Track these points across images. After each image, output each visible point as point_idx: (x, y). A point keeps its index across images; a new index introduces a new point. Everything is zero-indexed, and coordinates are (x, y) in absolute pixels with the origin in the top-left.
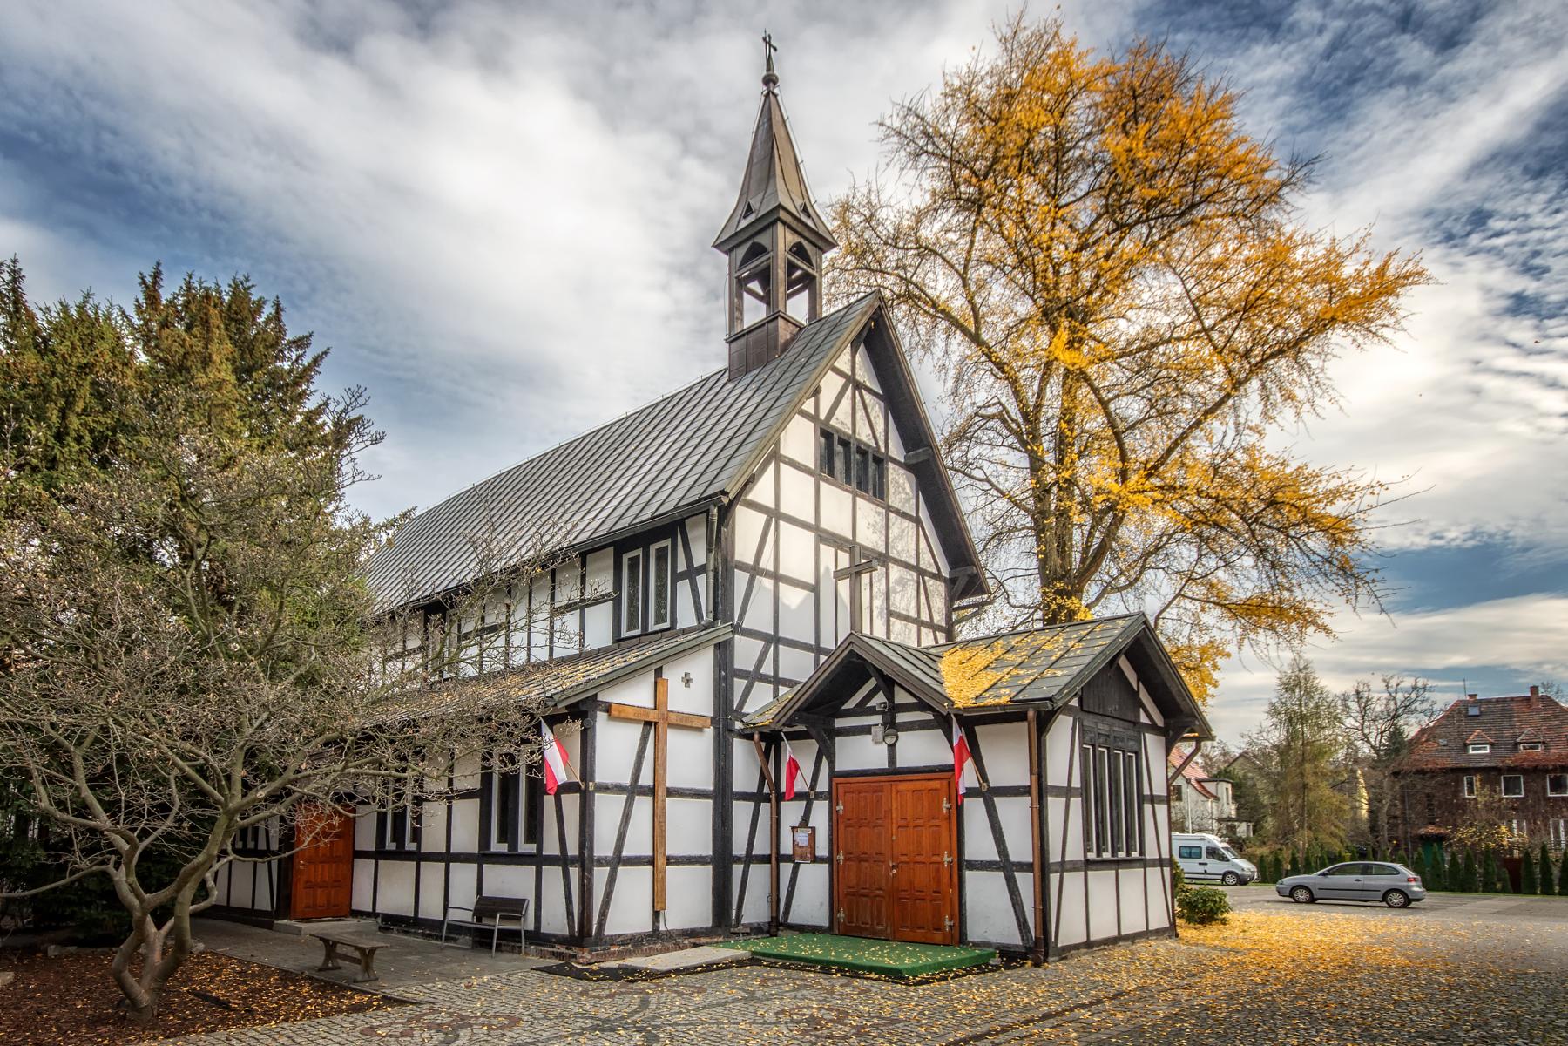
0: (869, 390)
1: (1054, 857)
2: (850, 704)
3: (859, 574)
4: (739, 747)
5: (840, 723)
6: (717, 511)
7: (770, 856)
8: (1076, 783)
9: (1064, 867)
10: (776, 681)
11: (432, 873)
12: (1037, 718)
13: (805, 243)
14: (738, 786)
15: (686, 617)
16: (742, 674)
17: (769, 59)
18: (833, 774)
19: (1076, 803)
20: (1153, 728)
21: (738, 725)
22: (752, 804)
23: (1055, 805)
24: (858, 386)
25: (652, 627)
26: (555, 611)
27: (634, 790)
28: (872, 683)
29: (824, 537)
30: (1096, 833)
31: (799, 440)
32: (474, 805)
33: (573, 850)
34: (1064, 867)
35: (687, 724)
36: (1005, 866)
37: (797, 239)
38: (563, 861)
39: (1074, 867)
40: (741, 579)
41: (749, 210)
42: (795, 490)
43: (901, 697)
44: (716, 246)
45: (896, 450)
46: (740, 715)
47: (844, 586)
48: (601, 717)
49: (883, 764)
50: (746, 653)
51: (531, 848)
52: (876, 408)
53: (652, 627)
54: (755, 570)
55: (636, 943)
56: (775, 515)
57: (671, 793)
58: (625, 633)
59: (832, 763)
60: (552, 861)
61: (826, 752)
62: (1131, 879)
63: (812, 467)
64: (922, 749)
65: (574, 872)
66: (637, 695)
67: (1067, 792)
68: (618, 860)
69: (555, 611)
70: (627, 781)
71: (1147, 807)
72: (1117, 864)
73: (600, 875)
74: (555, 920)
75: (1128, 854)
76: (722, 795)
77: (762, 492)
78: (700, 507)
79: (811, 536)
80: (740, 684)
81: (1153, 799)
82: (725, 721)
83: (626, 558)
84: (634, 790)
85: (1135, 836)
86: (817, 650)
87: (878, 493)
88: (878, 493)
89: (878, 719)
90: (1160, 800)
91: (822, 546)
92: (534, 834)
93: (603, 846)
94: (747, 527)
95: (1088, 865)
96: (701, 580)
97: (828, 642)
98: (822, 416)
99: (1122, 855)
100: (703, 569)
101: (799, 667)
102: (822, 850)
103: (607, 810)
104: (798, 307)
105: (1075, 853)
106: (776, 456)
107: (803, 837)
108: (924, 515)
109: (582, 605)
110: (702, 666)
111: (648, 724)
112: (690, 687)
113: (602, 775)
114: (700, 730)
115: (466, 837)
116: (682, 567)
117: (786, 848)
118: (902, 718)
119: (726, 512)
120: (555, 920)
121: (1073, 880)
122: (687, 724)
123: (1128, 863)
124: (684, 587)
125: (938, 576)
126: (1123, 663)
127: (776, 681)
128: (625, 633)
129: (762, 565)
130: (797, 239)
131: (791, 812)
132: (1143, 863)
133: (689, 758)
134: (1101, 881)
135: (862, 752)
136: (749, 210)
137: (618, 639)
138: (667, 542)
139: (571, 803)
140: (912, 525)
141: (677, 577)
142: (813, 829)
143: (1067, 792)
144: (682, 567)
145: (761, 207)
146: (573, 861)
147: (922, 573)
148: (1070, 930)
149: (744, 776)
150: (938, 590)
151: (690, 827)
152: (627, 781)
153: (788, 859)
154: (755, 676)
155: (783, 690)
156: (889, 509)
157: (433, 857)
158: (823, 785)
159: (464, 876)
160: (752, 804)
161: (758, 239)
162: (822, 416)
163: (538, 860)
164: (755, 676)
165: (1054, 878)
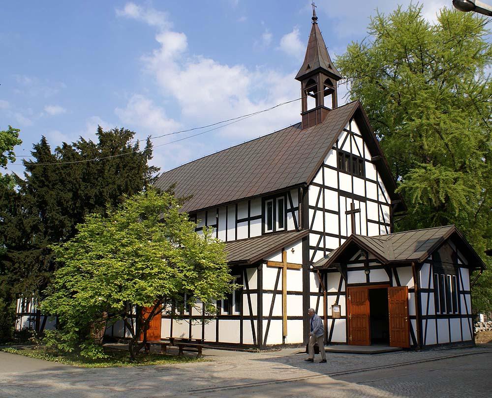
0: (357, 135)
1: (424, 313)
2: (353, 259)
3: (354, 213)
4: (312, 275)
5: (349, 266)
6: (302, 190)
8: (432, 287)
9: (428, 317)
10: (324, 249)
12: (415, 266)
13: (330, 79)
14: (311, 291)
15: (291, 226)
16: (312, 248)
17: (314, 11)
18: (347, 285)
19: (432, 295)
20: (464, 266)
21: (311, 267)
22: (317, 297)
23: (424, 296)
24: (353, 134)
25: (278, 229)
26: (237, 221)
27: (275, 292)
28: (359, 252)
29: (341, 193)
31: (332, 159)
33: (255, 313)
34: (428, 317)
35: (293, 267)
37: (327, 78)
38: (251, 318)
39: (432, 317)
40: (311, 212)
41: (309, 67)
42: (330, 177)
43: (371, 257)
44: (297, 78)
45: (368, 156)
46: (312, 263)
47: (349, 216)
48: (264, 266)
49: (300, 323)
50: (313, 240)
51: (237, 313)
52: (360, 141)
53: (278, 229)
54: (316, 208)
55: (276, 347)
56: (323, 187)
57: (289, 293)
58: (267, 231)
59: (346, 281)
60: (464, 316)
61: (345, 277)
62: (455, 322)
63: (336, 167)
64: (378, 276)
65: (255, 322)
66: (278, 258)
67: (428, 291)
68: (271, 318)
69: (237, 221)
70: (273, 289)
71: (462, 296)
72: (449, 317)
73: (265, 322)
74: (248, 340)
76: (306, 294)
77: (318, 180)
78: (297, 186)
79: (336, 193)
80: (311, 252)
81: (464, 293)
82: (307, 265)
83: (266, 202)
84: (275, 292)
85: (457, 306)
86: (340, 237)
87: (361, 174)
88: (361, 174)
89: (362, 265)
90: (467, 292)
91: (341, 197)
92: (240, 308)
93: (266, 313)
94: (313, 191)
96: (296, 213)
97: (343, 234)
98: (339, 147)
99: (451, 313)
100: (297, 209)
101: (333, 244)
102: (343, 314)
103: (267, 298)
104: (328, 102)
105: (432, 312)
106: (323, 165)
107: (337, 310)
108: (380, 180)
109: (249, 219)
110: (299, 247)
111: (280, 268)
112: (295, 255)
113: (265, 287)
114: (298, 270)
116: (289, 207)
117: (330, 314)
118: (372, 264)
119: (306, 190)
120: (248, 340)
121: (432, 322)
122: (293, 267)
123: (454, 316)
124: (290, 214)
125: (386, 204)
127: (324, 249)
128: (267, 231)
129: (313, 211)
130: (327, 78)
131: (332, 300)
132: (460, 316)
133: (294, 281)
134: (443, 322)
135: (357, 277)
136: (309, 67)
137: (264, 234)
138: (283, 197)
139: (254, 297)
140: (376, 185)
141: (287, 211)
142: (340, 306)
143: (428, 291)
144: (289, 207)
145: (314, 67)
146: (255, 318)
147: (380, 203)
148: (430, 340)
149: (314, 288)
150: (386, 209)
151: (295, 306)
152: (273, 289)
153: (330, 317)
154: (317, 248)
155: (327, 253)
156: (366, 180)
158: (343, 289)
160: (317, 297)
161: (312, 78)
162: (339, 147)
163: (241, 318)
164: (317, 248)
165: (424, 321)
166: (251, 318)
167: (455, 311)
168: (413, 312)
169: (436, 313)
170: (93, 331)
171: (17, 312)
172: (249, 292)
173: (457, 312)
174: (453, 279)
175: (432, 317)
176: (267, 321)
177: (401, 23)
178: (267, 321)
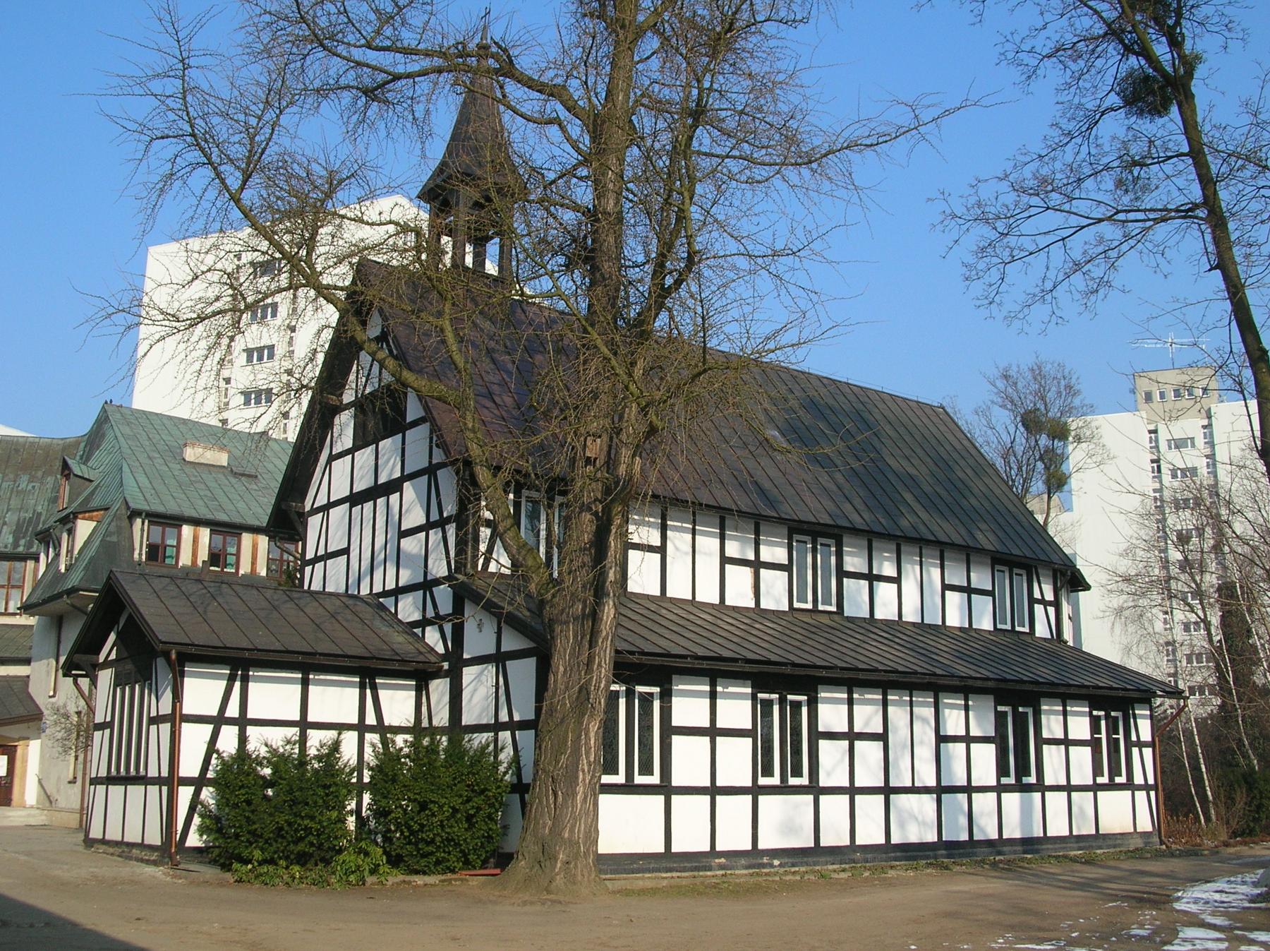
32: (1087, 751)
33: (165, 773)
38: (158, 781)
65: (165, 789)
72: (126, 780)
75: (1111, 778)
105: (103, 773)
115: (985, 772)
120: (154, 838)
139: (166, 728)
159: (1083, 800)
166: (158, 781)
169: (1094, 780)
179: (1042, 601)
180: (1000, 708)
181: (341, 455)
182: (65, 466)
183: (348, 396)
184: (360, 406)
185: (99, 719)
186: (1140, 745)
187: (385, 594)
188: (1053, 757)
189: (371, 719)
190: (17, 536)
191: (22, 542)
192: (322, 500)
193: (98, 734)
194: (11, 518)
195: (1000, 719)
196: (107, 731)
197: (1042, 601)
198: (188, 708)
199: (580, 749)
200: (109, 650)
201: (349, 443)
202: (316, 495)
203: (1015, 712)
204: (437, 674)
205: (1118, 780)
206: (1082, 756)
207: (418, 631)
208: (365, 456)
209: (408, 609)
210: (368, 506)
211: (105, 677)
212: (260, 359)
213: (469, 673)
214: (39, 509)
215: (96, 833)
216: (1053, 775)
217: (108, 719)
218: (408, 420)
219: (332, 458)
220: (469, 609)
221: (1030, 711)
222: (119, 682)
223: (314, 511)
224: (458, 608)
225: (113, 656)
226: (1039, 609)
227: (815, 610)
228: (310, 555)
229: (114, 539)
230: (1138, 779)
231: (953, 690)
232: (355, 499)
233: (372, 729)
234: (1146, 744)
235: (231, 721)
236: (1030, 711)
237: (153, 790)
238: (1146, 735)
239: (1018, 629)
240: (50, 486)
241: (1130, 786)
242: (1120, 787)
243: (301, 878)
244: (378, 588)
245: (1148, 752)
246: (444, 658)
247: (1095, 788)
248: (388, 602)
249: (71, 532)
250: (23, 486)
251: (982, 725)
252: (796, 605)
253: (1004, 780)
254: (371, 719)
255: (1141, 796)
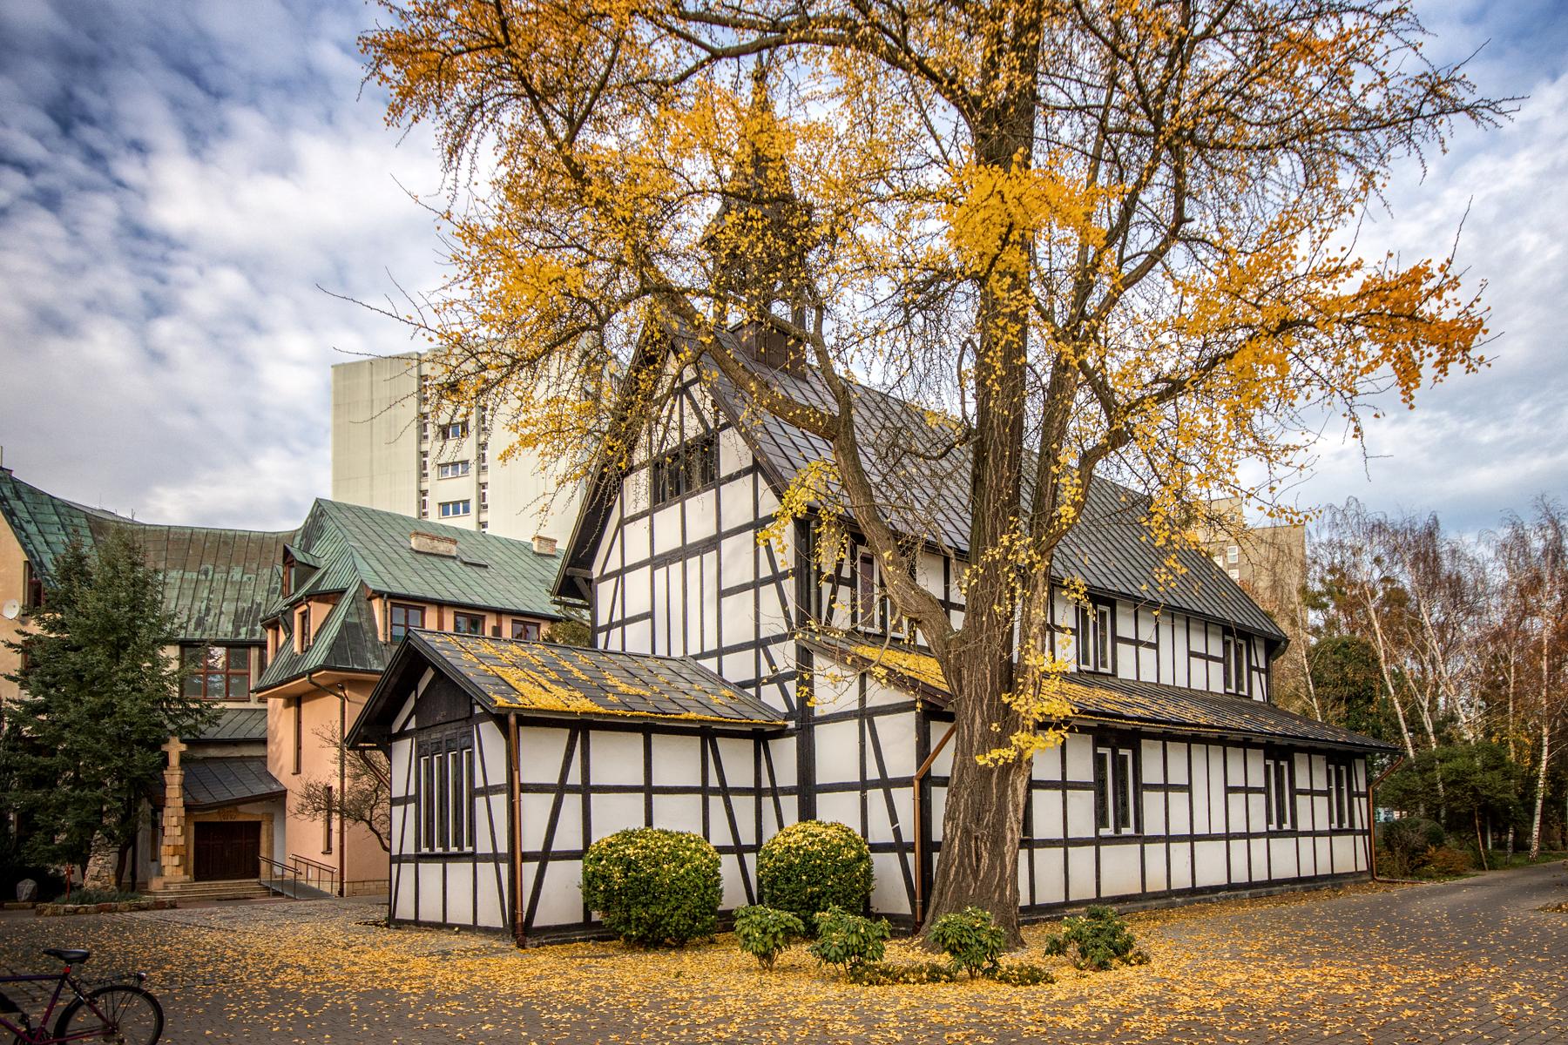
7: (913, 844)
11: (1155, 852)
19: (411, 807)
30: (426, 833)
32: (1089, 795)
33: (503, 848)
36: (899, 847)
38: (495, 858)
39: (408, 859)
60: (485, 858)
62: (460, 873)
65: (504, 867)
70: (655, 783)
72: (445, 858)
73: (529, 870)
75: (1117, 830)
93: (532, 840)
95: (419, 858)
103: (535, 810)
105: (409, 849)
115: (1082, 824)
120: (491, 915)
121: (408, 869)
126: (429, 675)
132: (474, 858)
134: (431, 872)
143: (487, 791)
152: (655, 783)
157: (1154, 839)
159: (1082, 858)
166: (495, 858)
167: (1122, 820)
168: (939, 796)
169: (1097, 831)
170: (1329, 290)
171: (1024, 900)
172: (487, 791)
173: (1126, 825)
174: (1120, 764)
175: (408, 859)
176: (762, 576)
177: (839, 70)
178: (762, 576)
179: (1257, 669)
180: (1100, 750)
181: (634, 519)
182: (287, 553)
183: (640, 456)
184: (657, 466)
185: (398, 791)
186: (1359, 795)
187: (704, 655)
188: (1046, 807)
189: (714, 782)
190: (237, 621)
191: (243, 630)
192: (614, 564)
193: (398, 811)
194: (228, 607)
195: (1099, 761)
196: (411, 807)
197: (1257, 669)
198: (528, 775)
199: (1006, 808)
200: (405, 717)
201: (644, 504)
202: (607, 559)
203: (1115, 753)
204: (781, 733)
205: (1125, 831)
206: (1082, 804)
207: (752, 691)
208: (668, 518)
209: (739, 667)
210: (676, 568)
211: (404, 750)
212: (456, 434)
213: (822, 734)
214: (258, 599)
215: (405, 910)
216: (1153, 825)
217: (412, 792)
218: (723, 475)
219: (622, 523)
220: (818, 661)
221: (1128, 753)
222: (421, 751)
223: (604, 578)
224: (805, 656)
225: (412, 725)
226: (1255, 674)
227: (1236, 695)
228: (603, 620)
229: (355, 620)
230: (1358, 826)
231: (1236, 744)
232: (657, 562)
233: (715, 791)
234: (788, 791)
235: (574, 789)
236: (1128, 753)
237: (486, 870)
238: (1362, 789)
239: (1101, 670)
240: (266, 577)
241: (1351, 831)
242: (1127, 840)
243: (860, 954)
244: (694, 649)
245: (1363, 800)
246: (787, 717)
247: (1098, 841)
248: (711, 664)
249: (305, 616)
250: (237, 577)
251: (1081, 767)
252: (1083, 667)
253: (1103, 832)
254: (714, 782)
255: (1359, 838)
